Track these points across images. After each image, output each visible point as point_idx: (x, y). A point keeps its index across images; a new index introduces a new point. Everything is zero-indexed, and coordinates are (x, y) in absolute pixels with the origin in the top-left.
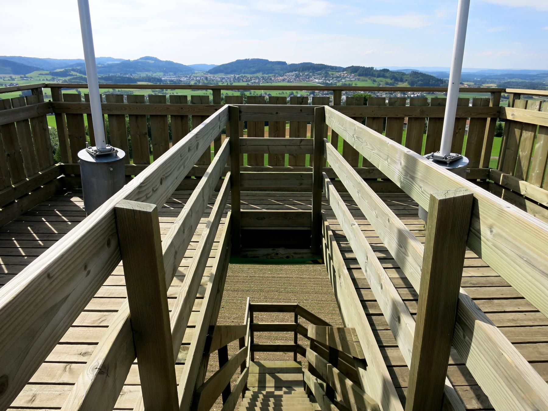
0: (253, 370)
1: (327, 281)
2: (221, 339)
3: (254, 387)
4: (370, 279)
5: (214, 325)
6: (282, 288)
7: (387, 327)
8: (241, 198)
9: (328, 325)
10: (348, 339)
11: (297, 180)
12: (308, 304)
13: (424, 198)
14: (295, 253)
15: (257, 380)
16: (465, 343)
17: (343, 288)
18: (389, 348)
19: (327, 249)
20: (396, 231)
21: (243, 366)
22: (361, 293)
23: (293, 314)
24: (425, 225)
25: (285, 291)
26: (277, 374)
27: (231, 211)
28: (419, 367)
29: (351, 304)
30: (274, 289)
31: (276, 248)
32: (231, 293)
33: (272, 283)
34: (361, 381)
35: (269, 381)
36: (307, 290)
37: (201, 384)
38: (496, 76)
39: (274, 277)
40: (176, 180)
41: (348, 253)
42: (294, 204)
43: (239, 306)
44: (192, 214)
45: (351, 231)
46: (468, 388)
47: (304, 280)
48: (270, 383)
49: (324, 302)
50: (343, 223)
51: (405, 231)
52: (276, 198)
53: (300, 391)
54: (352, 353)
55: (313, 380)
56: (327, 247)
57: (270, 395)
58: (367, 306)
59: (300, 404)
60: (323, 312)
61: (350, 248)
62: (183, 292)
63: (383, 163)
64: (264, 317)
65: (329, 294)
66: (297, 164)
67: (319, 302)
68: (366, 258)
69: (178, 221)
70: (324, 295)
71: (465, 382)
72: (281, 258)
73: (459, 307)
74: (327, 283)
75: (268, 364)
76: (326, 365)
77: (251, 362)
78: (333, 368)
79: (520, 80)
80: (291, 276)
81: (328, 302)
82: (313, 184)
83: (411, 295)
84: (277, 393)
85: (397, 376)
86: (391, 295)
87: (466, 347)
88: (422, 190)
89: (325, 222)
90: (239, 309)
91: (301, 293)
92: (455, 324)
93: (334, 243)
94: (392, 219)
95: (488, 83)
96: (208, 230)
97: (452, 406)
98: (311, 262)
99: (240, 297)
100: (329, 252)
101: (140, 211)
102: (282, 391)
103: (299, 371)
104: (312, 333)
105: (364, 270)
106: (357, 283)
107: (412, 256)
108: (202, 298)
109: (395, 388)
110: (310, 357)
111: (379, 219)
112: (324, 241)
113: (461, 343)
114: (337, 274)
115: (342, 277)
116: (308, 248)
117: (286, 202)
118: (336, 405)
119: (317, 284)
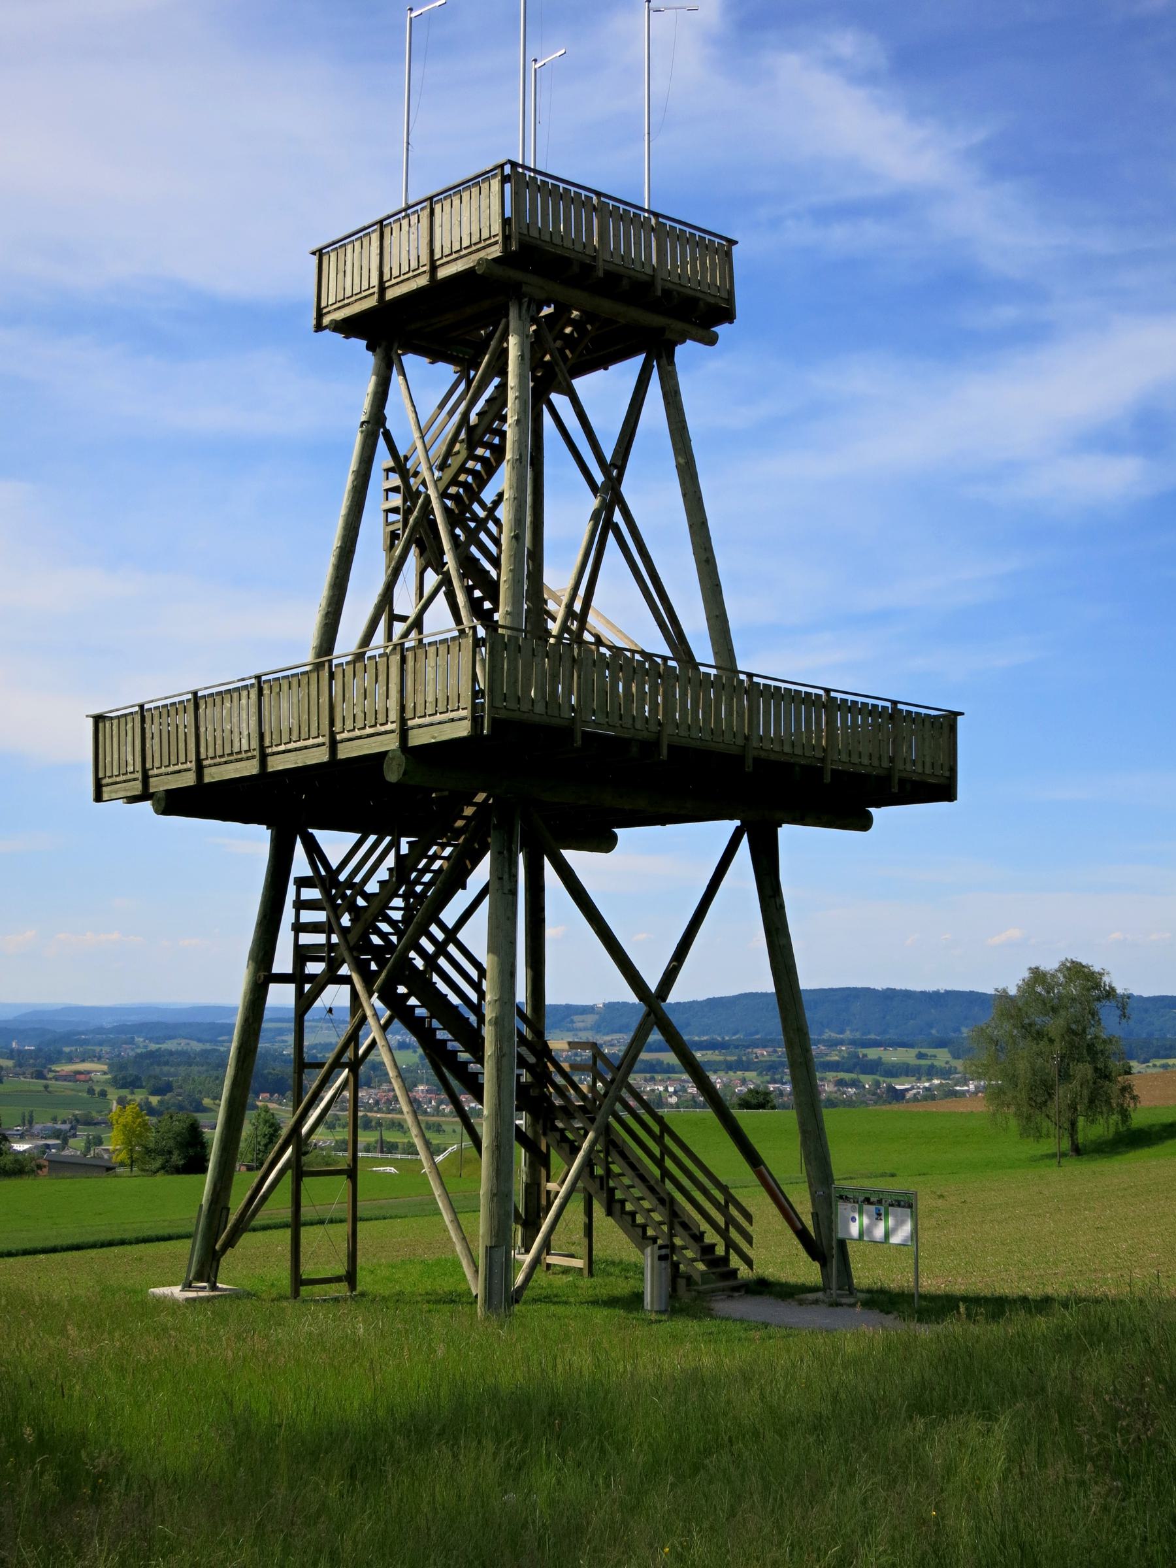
38: (100, 1030)
79: (197, 1046)
95: (70, 1060)
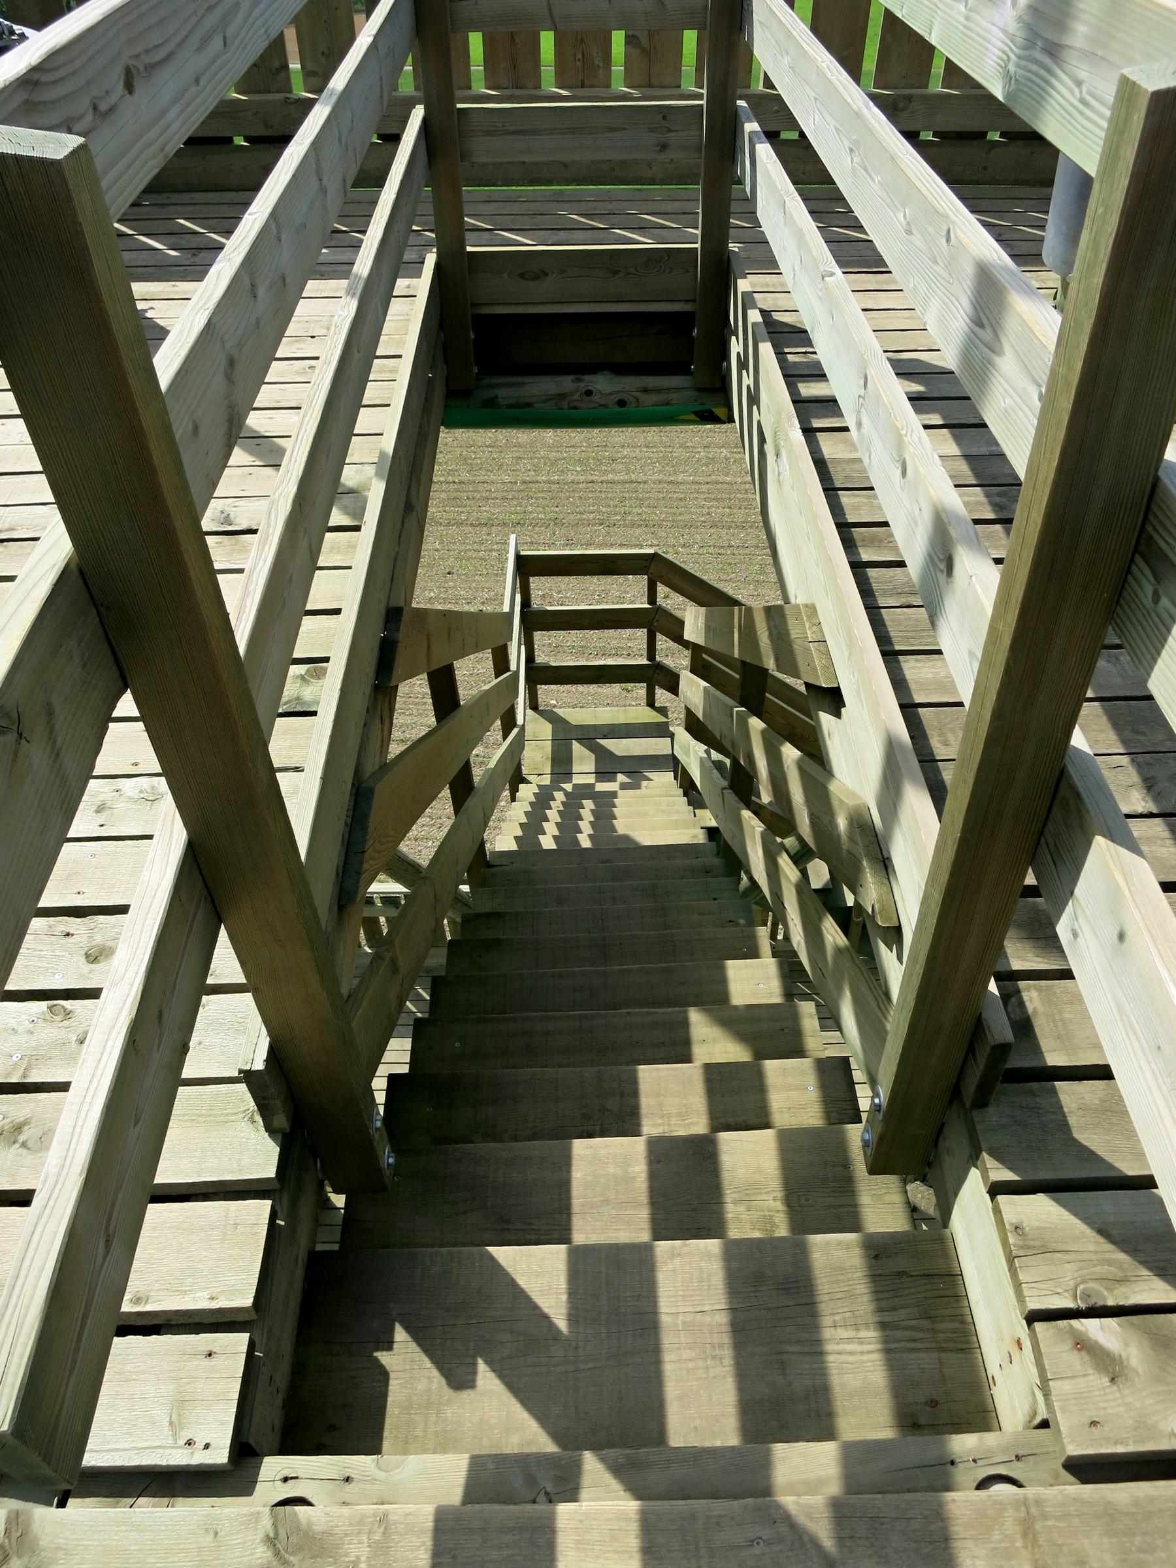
0: (539, 732)
1: (746, 490)
2: (429, 647)
3: (540, 775)
4: (869, 450)
5: (402, 604)
6: (616, 514)
7: (910, 599)
8: (467, 209)
9: (736, 603)
10: (793, 636)
11: (651, 130)
12: (690, 556)
13: (1084, 122)
14: (646, 390)
15: (548, 758)
16: (1157, 620)
17: (786, 487)
18: (909, 657)
19: (744, 372)
20: (969, 270)
21: (509, 722)
22: (840, 503)
23: (643, 580)
24: (1060, 289)
25: (624, 520)
26: (601, 741)
27: (435, 250)
28: (999, 693)
29: (808, 535)
30: (592, 516)
31: (584, 374)
32: (470, 533)
33: (587, 499)
34: (825, 746)
35: (581, 758)
36: (687, 517)
37: (376, 767)
39: (592, 482)
40: (194, 89)
41: (809, 381)
42: (642, 228)
43: (496, 568)
44: (279, 232)
45: (820, 298)
46: (1125, 760)
47: (681, 487)
48: (584, 763)
49: (736, 552)
50: (797, 272)
51: (1002, 268)
52: (585, 207)
53: (664, 780)
54: (803, 674)
55: (696, 752)
56: (743, 365)
57: (586, 791)
58: (854, 540)
59: (663, 811)
60: (731, 579)
61: (818, 364)
62: (282, 499)
63: (948, 11)
64: (568, 595)
65: (751, 527)
66: (654, 81)
67: (723, 551)
68: (862, 383)
69: (229, 254)
70: (736, 531)
71: (1119, 744)
72: (601, 405)
73: (1153, 506)
74: (745, 496)
75: (577, 716)
76: (732, 710)
77: (529, 712)
78: (749, 717)
80: (642, 477)
81: (747, 551)
82: (703, 148)
83: (989, 508)
84: (602, 787)
85: (928, 732)
86: (933, 493)
87: (1157, 632)
88: (1081, 92)
89: (738, 280)
90: (496, 575)
91: (670, 525)
92: (1132, 561)
93: (766, 349)
94: (962, 231)
96: (354, 304)
97: (1084, 804)
98: (693, 417)
99: (497, 543)
100: (748, 381)
101: (17, 158)
102: (615, 781)
103: (661, 731)
104: (695, 628)
105: (855, 420)
106: (829, 472)
107: (1016, 352)
108: (357, 528)
109: (920, 761)
110: (689, 694)
111: (917, 239)
112: (736, 347)
113: (1142, 620)
114: (769, 448)
115: (783, 453)
116: (685, 371)
117: (615, 219)
118: (755, 813)
119: (717, 500)
